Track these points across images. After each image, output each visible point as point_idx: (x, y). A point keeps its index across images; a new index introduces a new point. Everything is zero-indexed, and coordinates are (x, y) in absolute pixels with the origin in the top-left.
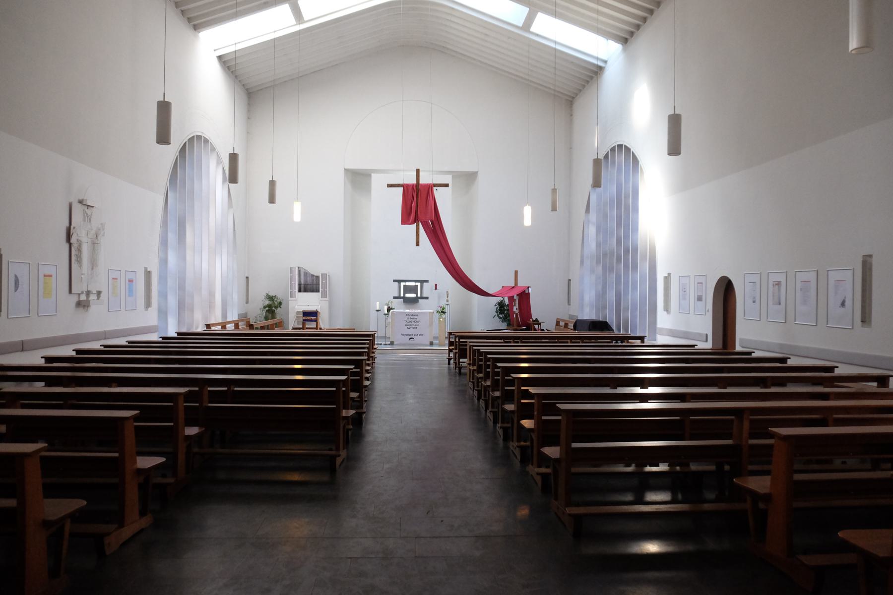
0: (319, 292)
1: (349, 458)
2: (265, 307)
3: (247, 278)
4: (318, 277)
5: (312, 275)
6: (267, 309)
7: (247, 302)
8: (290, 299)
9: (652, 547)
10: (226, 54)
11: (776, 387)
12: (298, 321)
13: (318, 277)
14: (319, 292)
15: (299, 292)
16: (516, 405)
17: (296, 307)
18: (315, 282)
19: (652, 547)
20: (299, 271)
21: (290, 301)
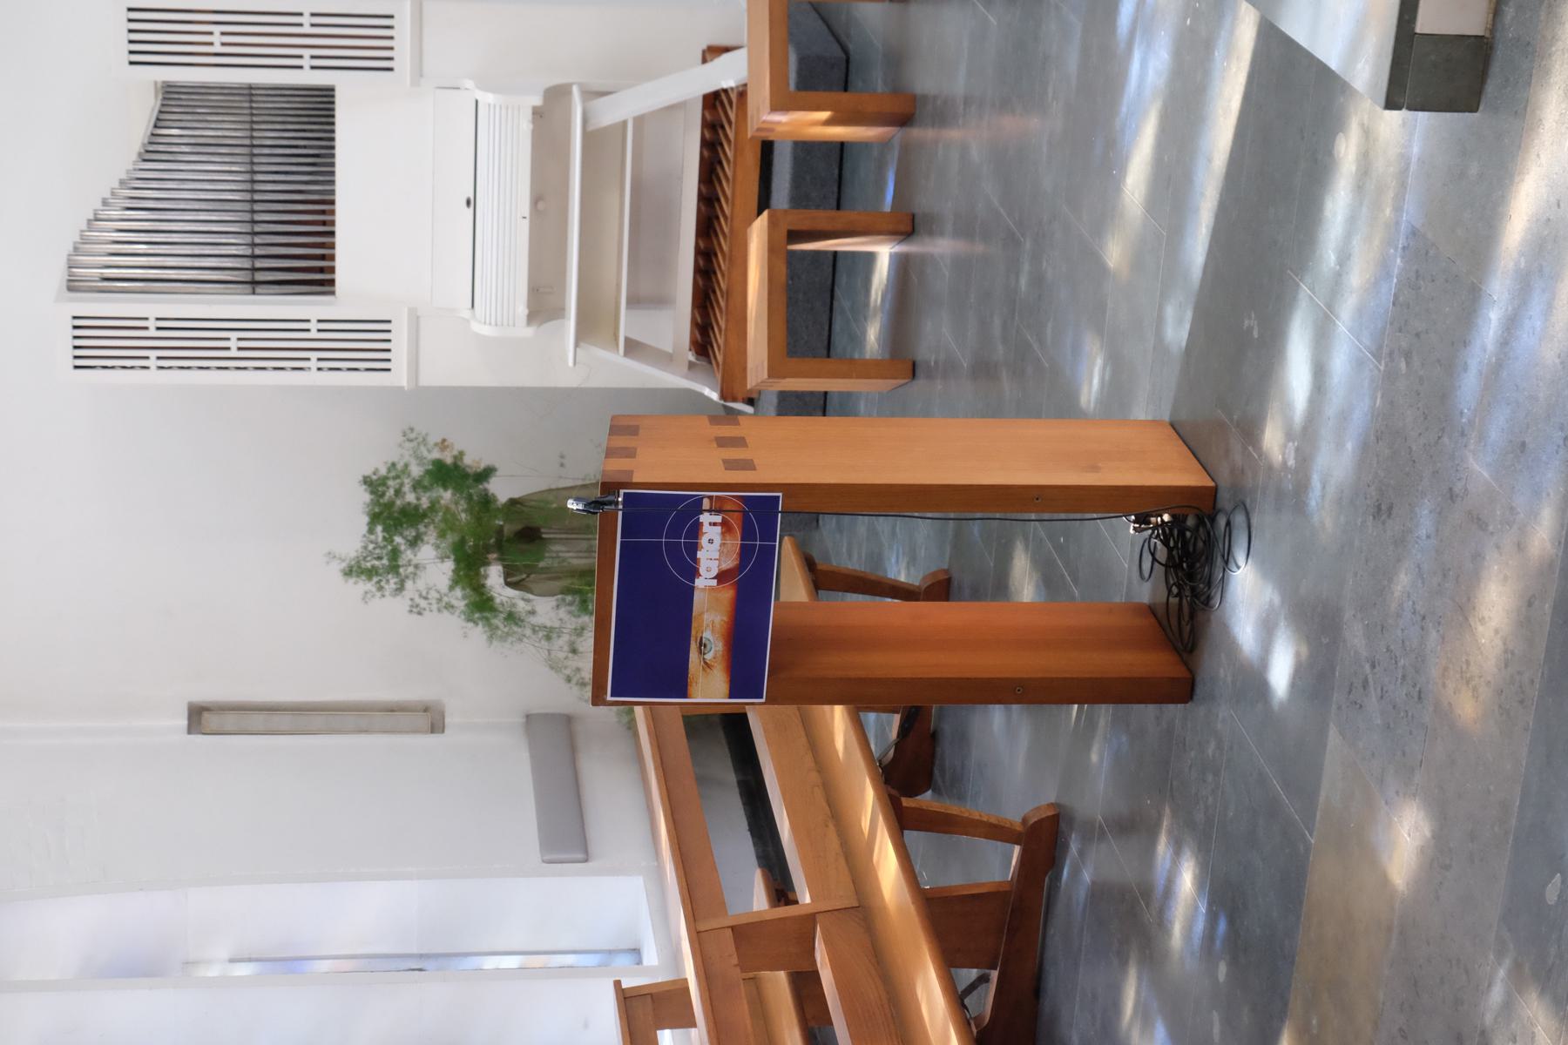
0: (327, 94)
1: (1553, 37)
2: (482, 605)
3: (199, 717)
4: (171, 94)
5: (150, 153)
6: (494, 576)
7: (432, 719)
8: (399, 376)
9: (1188, 22)
10: (649, 346)
11: (893, 812)
12: (635, 301)
13: (171, 94)
14: (327, 94)
15: (319, 279)
16: (768, 917)
17: (479, 328)
18: (229, 129)
19: (1188, 22)
20: (110, 284)
21: (427, 380)
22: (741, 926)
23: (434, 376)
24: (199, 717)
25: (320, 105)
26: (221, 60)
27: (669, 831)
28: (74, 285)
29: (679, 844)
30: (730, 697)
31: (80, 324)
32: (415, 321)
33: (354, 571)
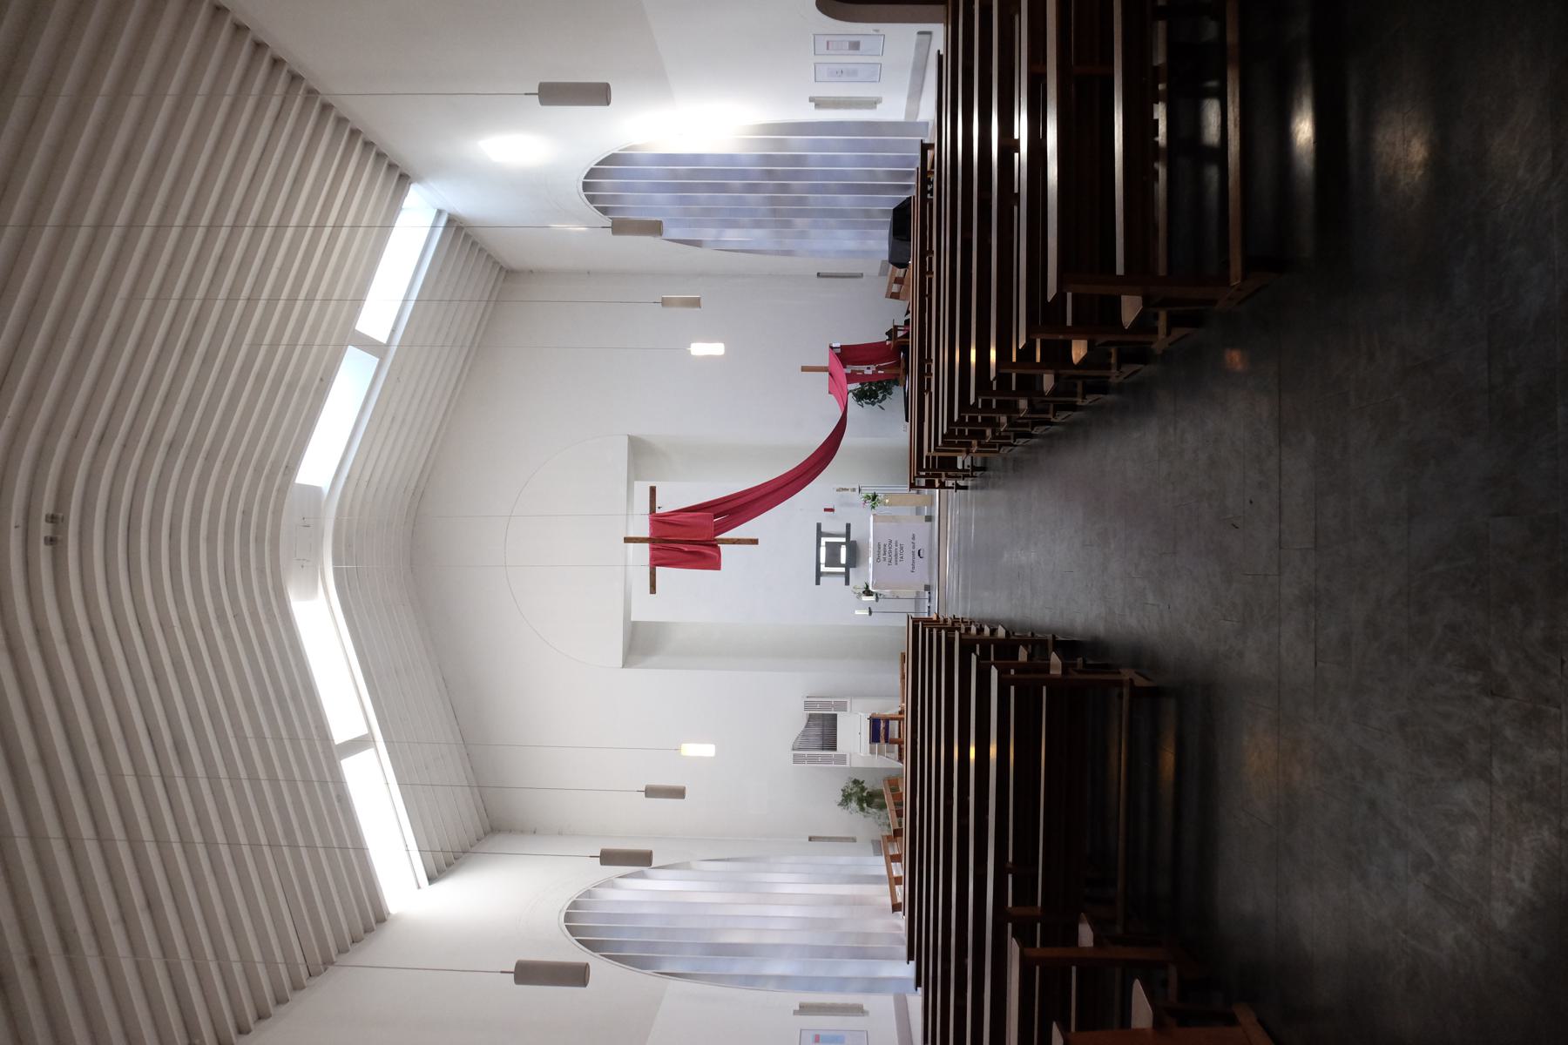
0: (836, 715)
1: (1136, 665)
2: (862, 809)
4: (810, 715)
5: (806, 727)
6: (865, 805)
7: (854, 840)
8: (848, 765)
9: (1304, 130)
15: (834, 748)
17: (862, 755)
19: (1304, 130)
20: (799, 749)
22: (633, 437)
23: (854, 765)
24: (810, 839)
25: (835, 717)
26: (820, 709)
27: (252, 316)
28: (793, 750)
29: (1316, 532)
30: (1034, 376)
31: (794, 755)
32: (850, 755)
33: (840, 804)
